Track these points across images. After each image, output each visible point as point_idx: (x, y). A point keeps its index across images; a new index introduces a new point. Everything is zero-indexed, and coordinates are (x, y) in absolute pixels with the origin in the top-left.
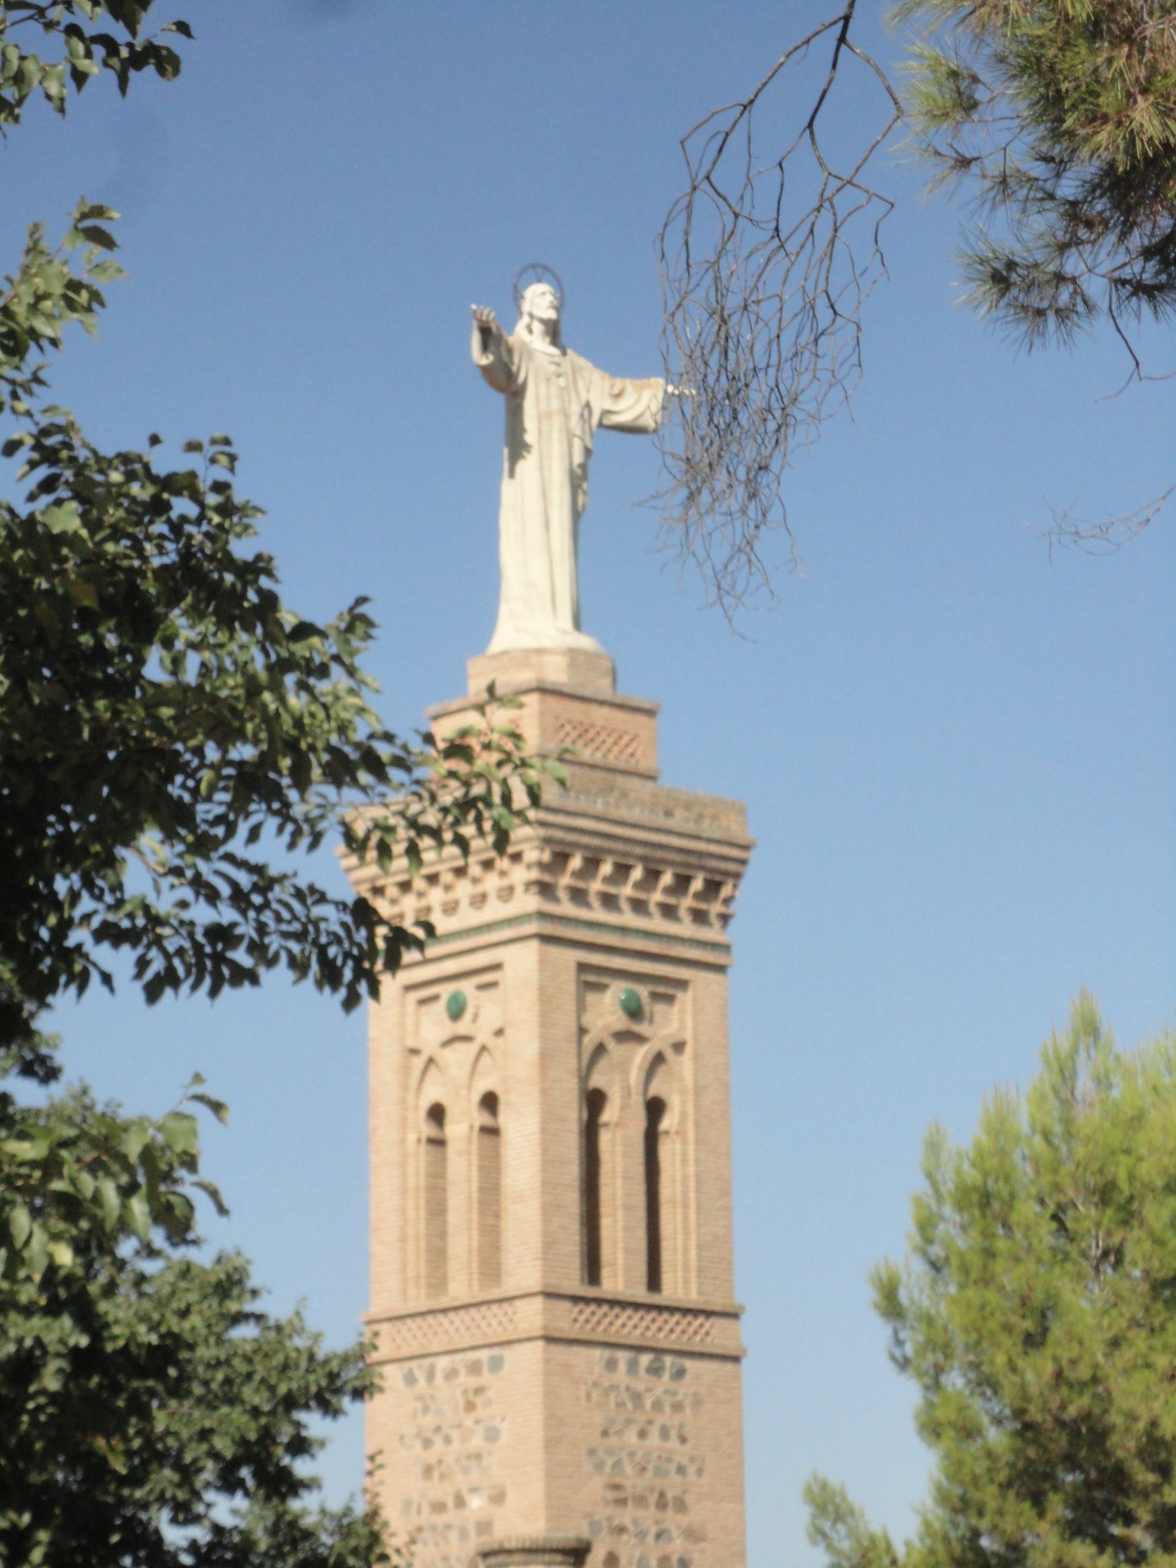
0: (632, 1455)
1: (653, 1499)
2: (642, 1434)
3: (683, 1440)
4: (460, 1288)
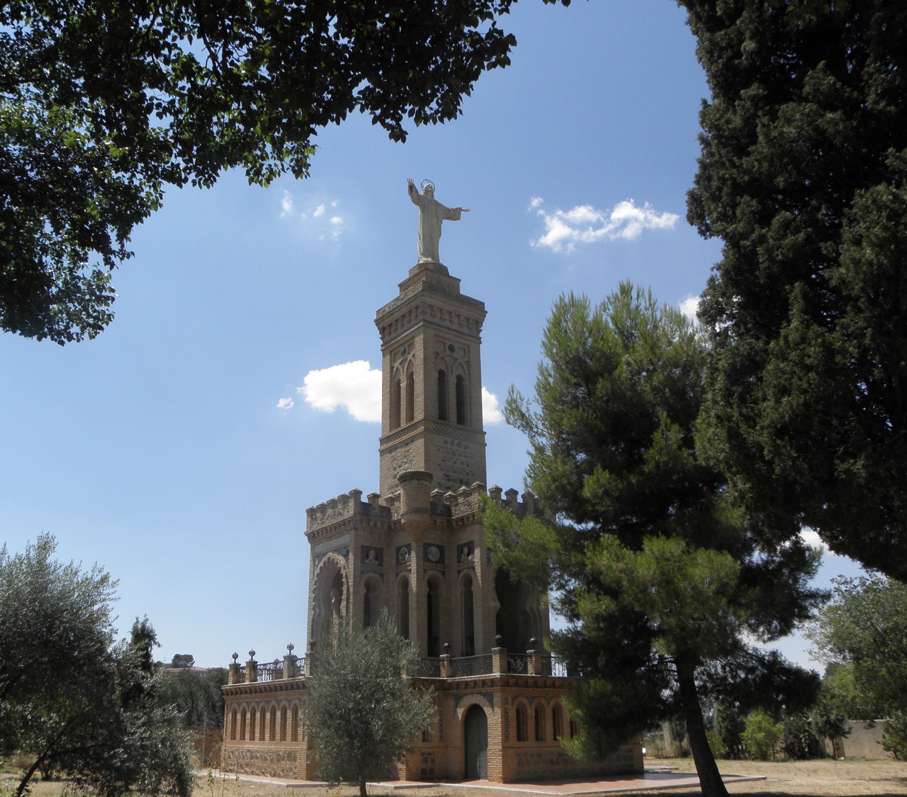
0: (452, 468)
3: (468, 466)
4: (403, 425)
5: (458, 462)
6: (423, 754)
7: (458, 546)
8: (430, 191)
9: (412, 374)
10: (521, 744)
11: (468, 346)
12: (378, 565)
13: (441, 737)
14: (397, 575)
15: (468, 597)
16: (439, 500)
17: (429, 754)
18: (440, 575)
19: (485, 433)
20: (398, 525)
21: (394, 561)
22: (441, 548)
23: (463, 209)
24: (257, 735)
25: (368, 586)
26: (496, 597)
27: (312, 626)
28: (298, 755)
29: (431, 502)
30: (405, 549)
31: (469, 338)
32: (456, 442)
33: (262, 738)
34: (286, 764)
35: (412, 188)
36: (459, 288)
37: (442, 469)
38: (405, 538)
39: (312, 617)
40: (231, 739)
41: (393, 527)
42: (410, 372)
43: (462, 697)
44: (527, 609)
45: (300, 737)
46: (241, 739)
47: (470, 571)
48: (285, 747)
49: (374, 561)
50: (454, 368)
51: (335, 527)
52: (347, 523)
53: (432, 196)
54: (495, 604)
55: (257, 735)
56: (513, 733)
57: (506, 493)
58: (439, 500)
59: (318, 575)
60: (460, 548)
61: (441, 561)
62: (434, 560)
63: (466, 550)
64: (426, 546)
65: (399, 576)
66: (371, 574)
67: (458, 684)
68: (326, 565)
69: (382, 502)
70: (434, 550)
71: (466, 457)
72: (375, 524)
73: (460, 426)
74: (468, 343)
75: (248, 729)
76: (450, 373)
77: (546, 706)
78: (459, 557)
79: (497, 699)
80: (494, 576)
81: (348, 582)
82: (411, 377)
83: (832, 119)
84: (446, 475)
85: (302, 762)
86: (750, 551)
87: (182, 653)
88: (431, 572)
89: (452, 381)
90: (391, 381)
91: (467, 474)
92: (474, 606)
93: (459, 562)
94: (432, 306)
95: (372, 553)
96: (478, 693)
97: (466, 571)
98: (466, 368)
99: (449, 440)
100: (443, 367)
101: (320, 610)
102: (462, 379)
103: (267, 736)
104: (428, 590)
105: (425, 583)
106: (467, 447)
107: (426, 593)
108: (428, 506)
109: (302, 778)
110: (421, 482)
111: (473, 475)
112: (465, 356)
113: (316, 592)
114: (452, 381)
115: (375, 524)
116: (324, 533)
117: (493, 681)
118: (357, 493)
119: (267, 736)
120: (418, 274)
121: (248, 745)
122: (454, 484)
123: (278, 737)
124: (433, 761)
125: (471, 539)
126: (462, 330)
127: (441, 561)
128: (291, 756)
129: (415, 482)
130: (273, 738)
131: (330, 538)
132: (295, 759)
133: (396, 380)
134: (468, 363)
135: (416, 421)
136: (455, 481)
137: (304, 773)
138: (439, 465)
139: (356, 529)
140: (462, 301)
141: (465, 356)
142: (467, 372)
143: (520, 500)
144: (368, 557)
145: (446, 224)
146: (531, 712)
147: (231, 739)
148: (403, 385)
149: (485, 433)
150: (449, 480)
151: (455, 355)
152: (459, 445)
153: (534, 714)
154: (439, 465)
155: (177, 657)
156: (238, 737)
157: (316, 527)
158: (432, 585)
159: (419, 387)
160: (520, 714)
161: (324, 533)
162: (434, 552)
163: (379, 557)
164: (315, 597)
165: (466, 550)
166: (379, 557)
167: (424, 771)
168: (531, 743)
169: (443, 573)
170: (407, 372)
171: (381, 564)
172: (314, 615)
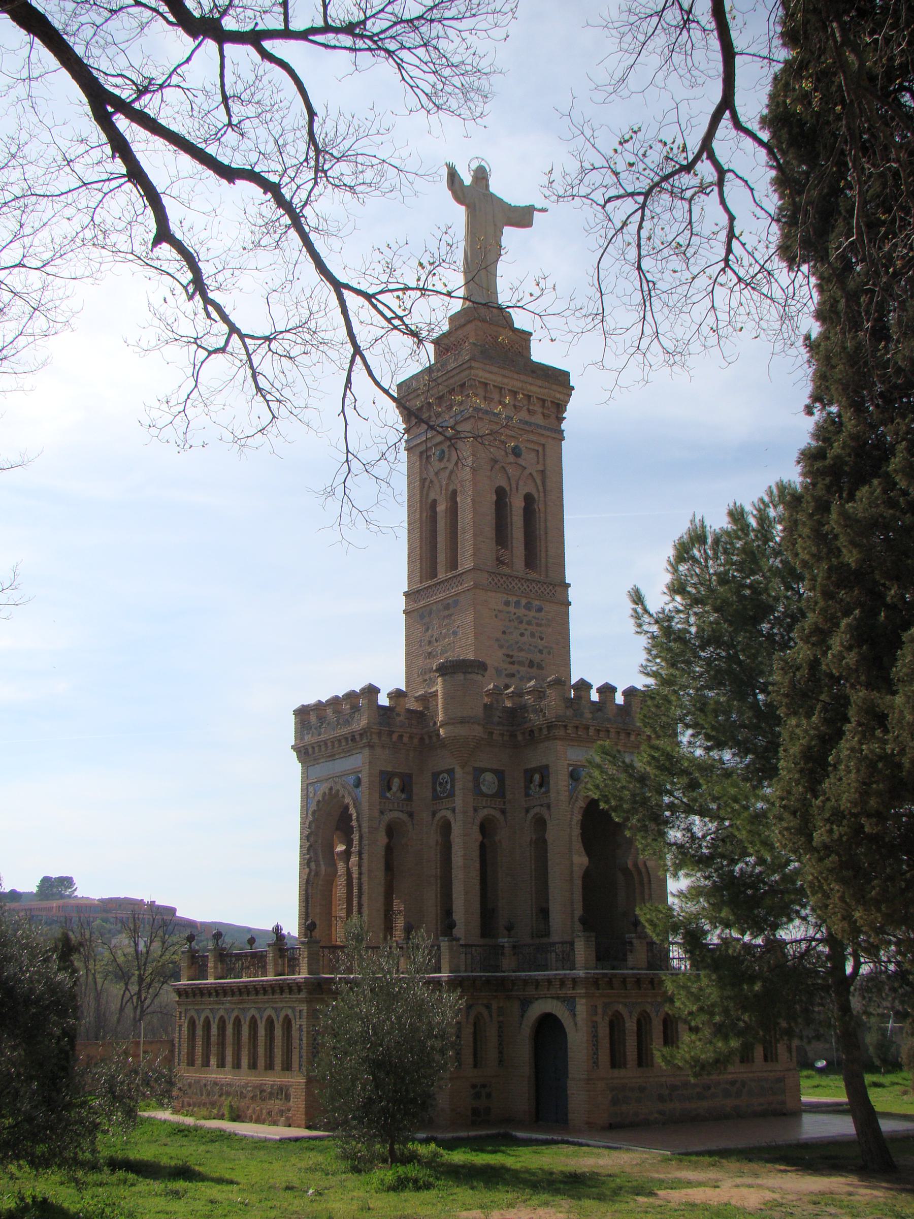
0: (517, 643)
1: (527, 663)
2: (522, 635)
3: (542, 639)
4: (441, 576)
5: (527, 633)
6: (474, 1086)
7: (526, 771)
8: (481, 175)
9: (454, 493)
10: (616, 1073)
11: (544, 445)
12: (404, 800)
13: (500, 1061)
14: (434, 814)
15: (541, 845)
16: (497, 701)
17: (484, 1086)
18: (497, 814)
19: (569, 585)
20: (434, 739)
21: (429, 794)
22: (500, 775)
23: (538, 206)
24: (229, 1059)
25: (391, 831)
26: (582, 849)
27: (307, 890)
28: (292, 1090)
29: (485, 705)
30: (446, 775)
31: (544, 432)
32: (524, 601)
33: (237, 1065)
34: (276, 1105)
35: (453, 177)
36: (528, 348)
37: (501, 647)
38: (444, 761)
39: (305, 877)
40: (188, 1065)
41: (427, 741)
42: (451, 488)
43: (531, 1002)
44: (630, 865)
45: (295, 1065)
46: (203, 1066)
47: (544, 811)
48: (271, 1080)
49: (399, 794)
50: (521, 483)
51: (340, 741)
52: (357, 737)
53: (487, 186)
54: (581, 860)
55: (229, 1059)
56: (604, 1057)
57: (599, 690)
58: (497, 701)
59: (314, 812)
60: (529, 775)
61: (501, 792)
62: (490, 793)
63: (537, 777)
64: (478, 772)
65: (438, 816)
66: (396, 814)
67: (526, 982)
68: (327, 797)
69: (413, 705)
70: (489, 777)
71: (538, 625)
72: (401, 736)
73: (533, 575)
74: (543, 441)
75: (214, 1049)
76: (514, 490)
77: (653, 1015)
78: (527, 788)
79: (581, 1007)
80: (580, 817)
81: (360, 826)
82: (453, 511)
83: (848, 494)
84: (508, 656)
85: (298, 1103)
86: (786, 913)
87: (54, 874)
88: (486, 812)
89: (517, 504)
90: (421, 501)
91: (541, 652)
92: (550, 863)
93: (527, 795)
94: (486, 384)
95: (396, 782)
96: (553, 998)
97: (537, 810)
98: (539, 482)
99: (513, 599)
100: (503, 483)
101: (318, 865)
102: (534, 499)
103: (245, 1062)
104: (480, 838)
105: (476, 828)
106: (540, 610)
107: (478, 844)
108: (479, 712)
109: (299, 1126)
110: (469, 676)
111: (549, 653)
112: (538, 463)
113: (312, 839)
114: (517, 504)
115: (401, 736)
116: (323, 749)
117: (575, 981)
118: (372, 691)
119: (245, 1062)
120: (464, 325)
121: (214, 1075)
122: (521, 669)
123: (261, 1062)
124: (489, 1096)
125: (544, 762)
126: (533, 420)
127: (501, 792)
128: (283, 1092)
129: (460, 677)
130: (253, 1066)
131: (332, 757)
132: (287, 1098)
133: (430, 501)
134: (543, 472)
135: (460, 570)
136: (521, 663)
137: (301, 1116)
138: (497, 640)
139: (371, 746)
140: (533, 372)
141: (538, 463)
142: (541, 488)
143: (619, 699)
144: (389, 789)
145: (510, 236)
146: (631, 1025)
147: (188, 1065)
148: (441, 508)
149: (569, 585)
150: (512, 663)
151: (521, 461)
152: (528, 607)
153: (635, 1028)
154: (497, 640)
155: (46, 880)
156: (199, 1061)
157: (308, 739)
158: (486, 828)
159: (466, 518)
160: (616, 1024)
161: (323, 749)
162: (489, 781)
163: (405, 788)
164: (310, 846)
165: (537, 777)
166: (405, 788)
167: (475, 1112)
168: (630, 1074)
169: (503, 812)
170: (447, 490)
171: (409, 799)
172: (309, 874)
